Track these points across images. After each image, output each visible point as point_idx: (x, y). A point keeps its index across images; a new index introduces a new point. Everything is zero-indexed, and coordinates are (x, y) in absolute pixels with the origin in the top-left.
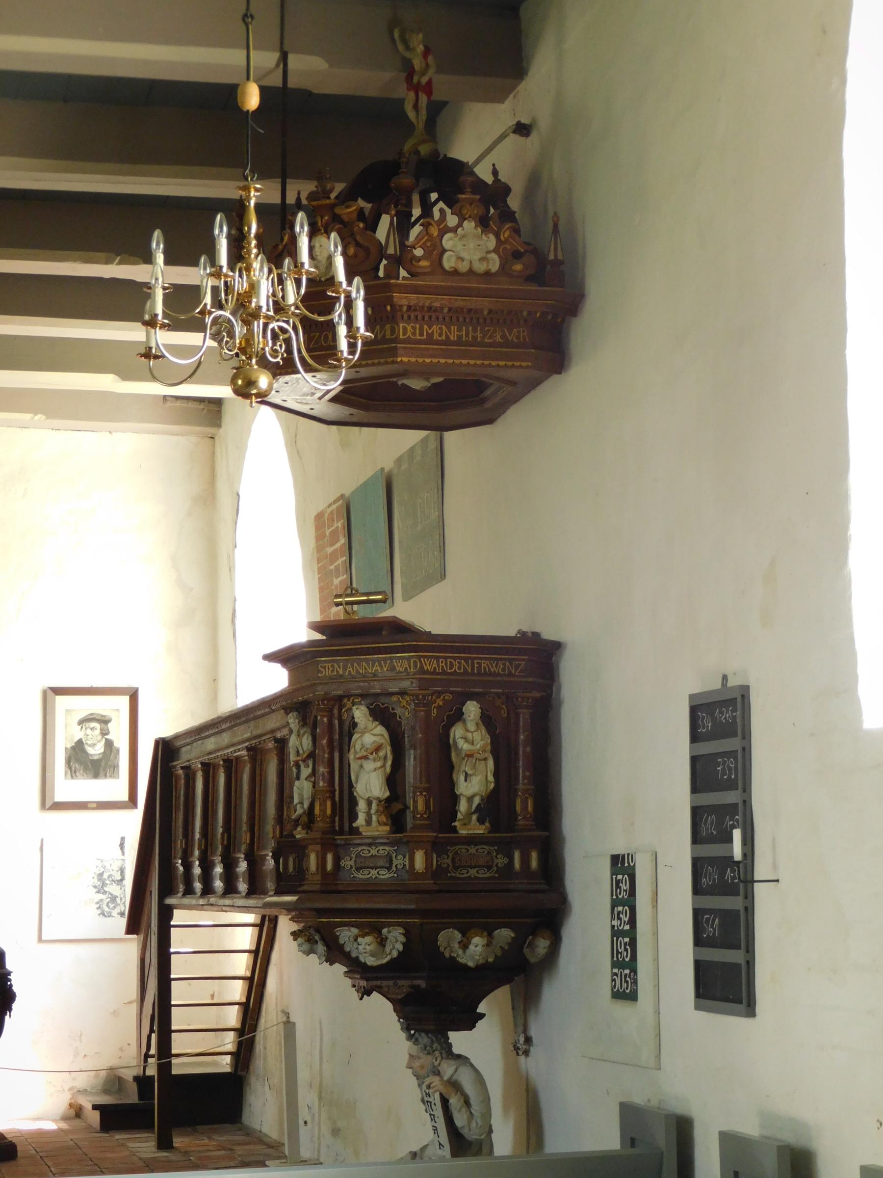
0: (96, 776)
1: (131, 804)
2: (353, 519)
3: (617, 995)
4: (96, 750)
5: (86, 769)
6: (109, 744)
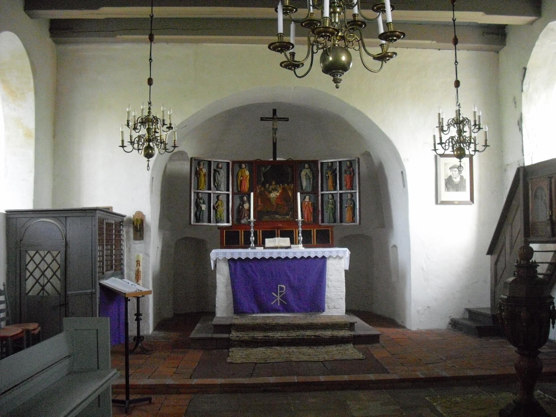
0: (457, 190)
1: (471, 203)
2: (189, 188)
3: (288, 121)
4: (457, 180)
5: (453, 188)
6: (462, 177)
